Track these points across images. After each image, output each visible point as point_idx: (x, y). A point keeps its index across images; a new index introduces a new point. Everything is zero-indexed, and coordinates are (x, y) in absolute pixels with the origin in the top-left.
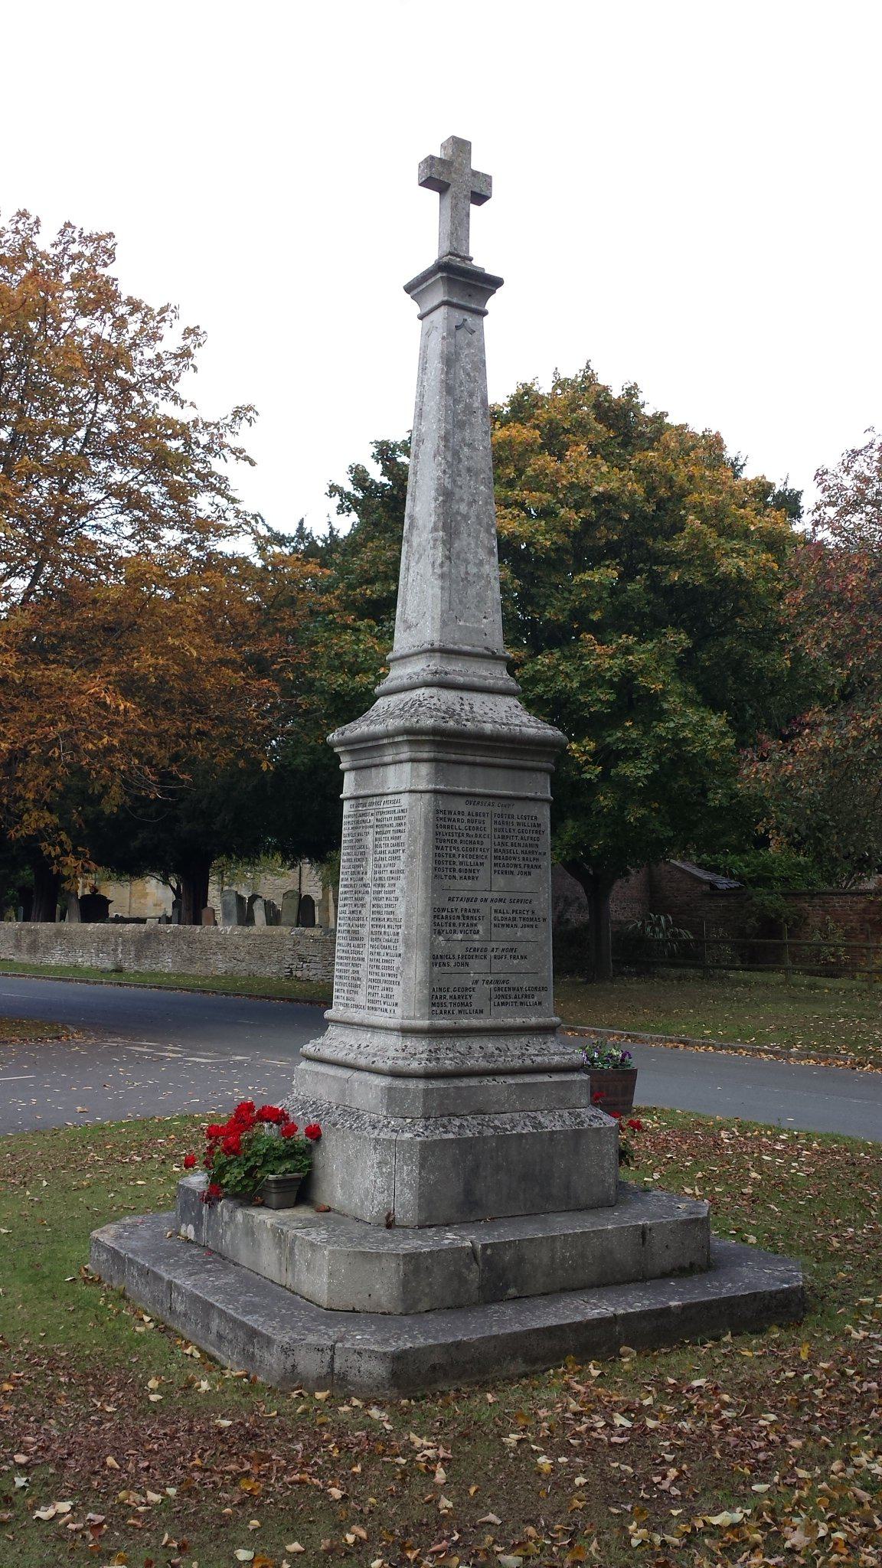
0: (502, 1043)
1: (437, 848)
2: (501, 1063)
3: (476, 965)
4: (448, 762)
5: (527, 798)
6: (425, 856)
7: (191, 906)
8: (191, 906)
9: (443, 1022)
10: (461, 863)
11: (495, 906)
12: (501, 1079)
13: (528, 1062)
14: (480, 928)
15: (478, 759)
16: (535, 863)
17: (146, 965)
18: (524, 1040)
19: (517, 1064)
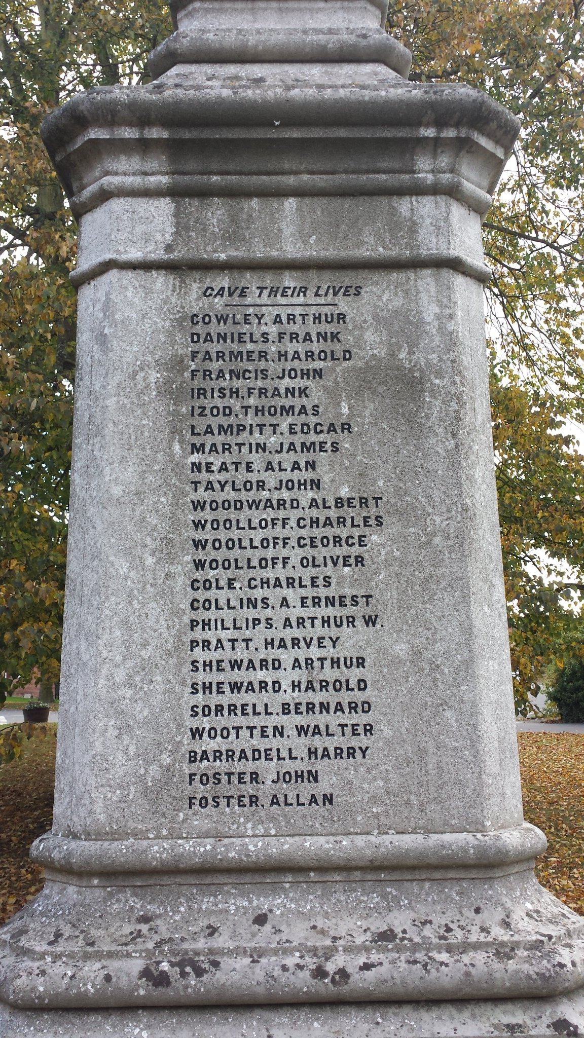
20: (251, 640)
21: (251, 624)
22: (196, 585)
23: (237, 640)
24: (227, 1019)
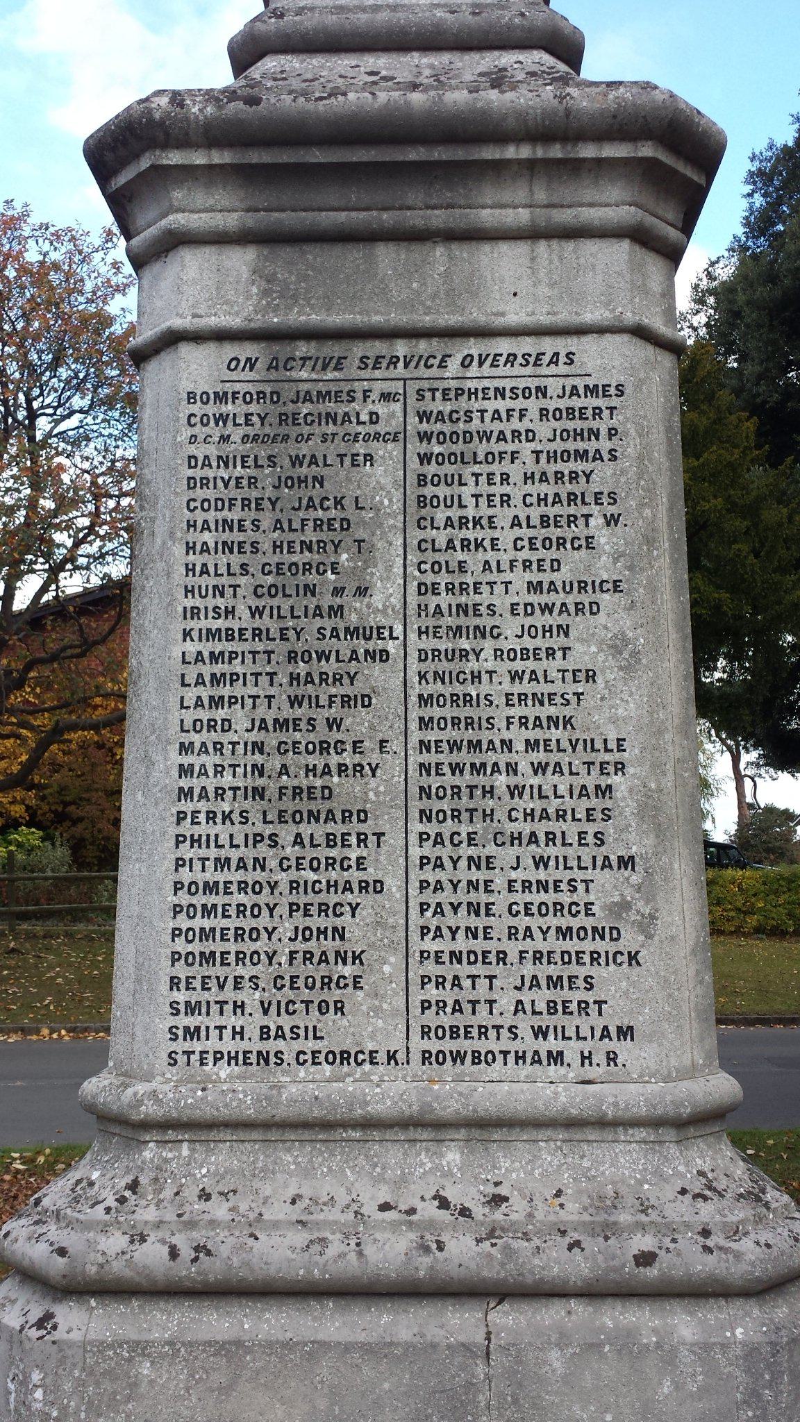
20: (606, 1002)
21: (251, 842)
22: (193, 420)
23: (259, 697)
24: (369, 1310)
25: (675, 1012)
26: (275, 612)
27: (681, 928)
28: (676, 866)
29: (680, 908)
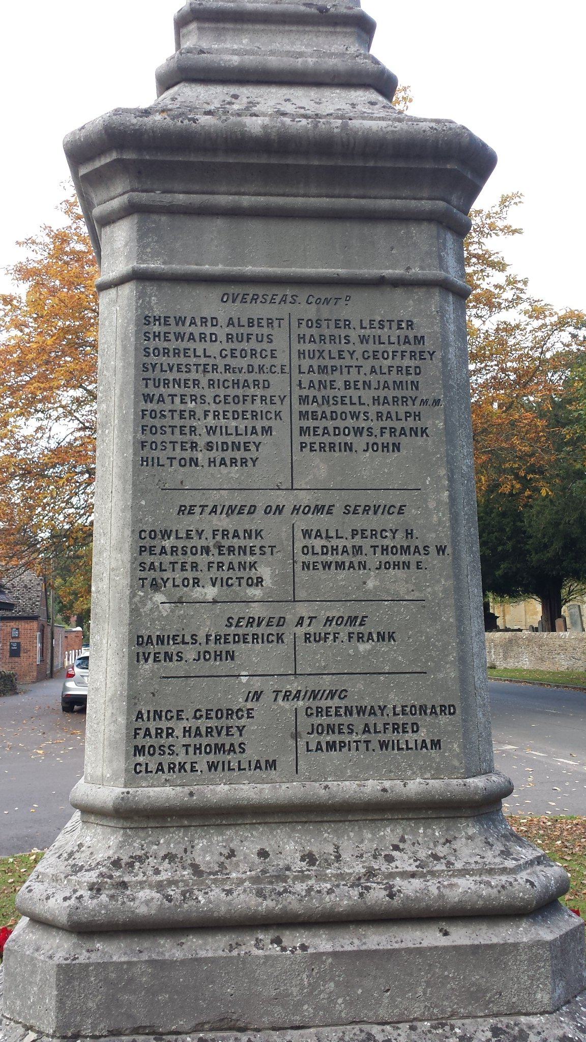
0: (322, 841)
1: (148, 398)
2: (296, 897)
3: (252, 655)
4: (172, 211)
5: (380, 283)
6: (123, 420)
7: (552, 618)
8: (552, 618)
9: (160, 792)
10: (211, 430)
11: (302, 522)
12: (294, 939)
13: (377, 895)
14: (264, 571)
15: (246, 201)
16: (411, 423)
17: (511, 664)
18: (389, 833)
19: (345, 898)
25: (93, 739)
26: (224, 430)
27: (104, 683)
28: (104, 641)
29: (104, 670)
